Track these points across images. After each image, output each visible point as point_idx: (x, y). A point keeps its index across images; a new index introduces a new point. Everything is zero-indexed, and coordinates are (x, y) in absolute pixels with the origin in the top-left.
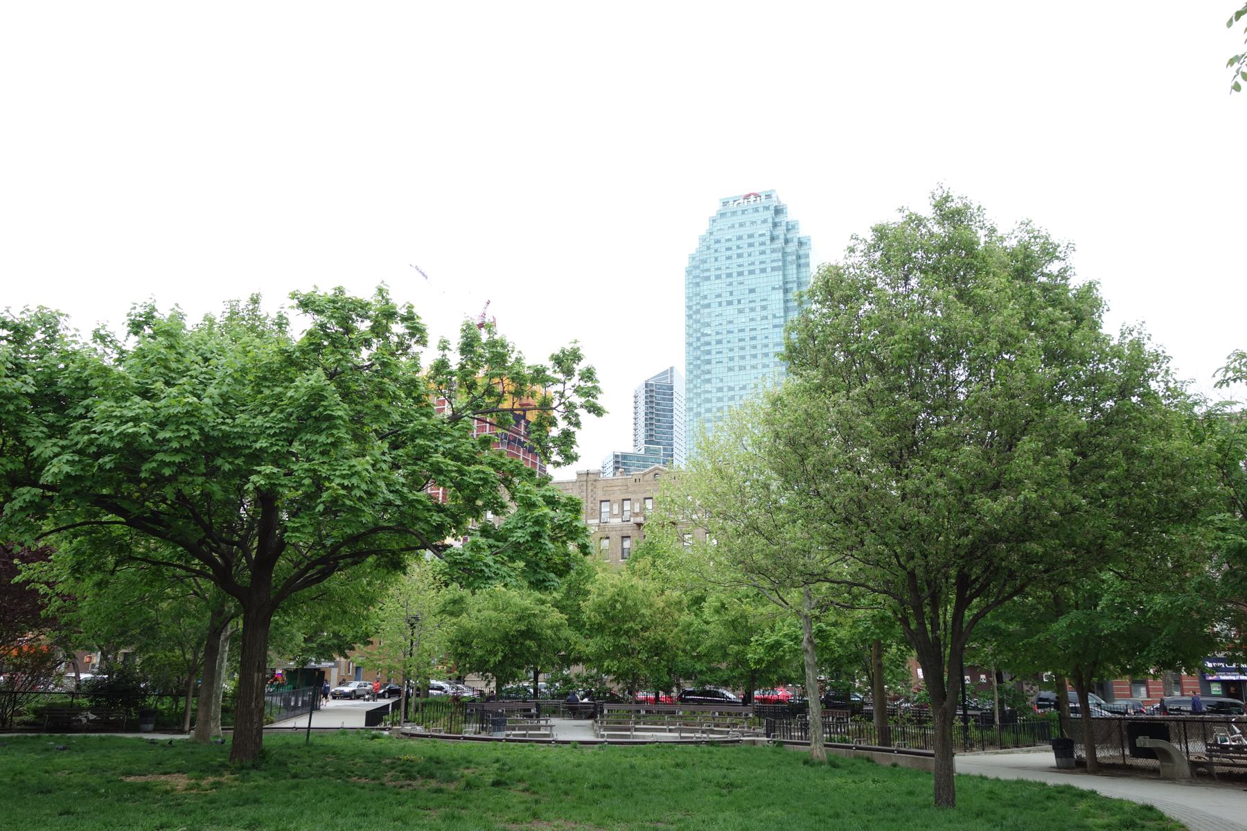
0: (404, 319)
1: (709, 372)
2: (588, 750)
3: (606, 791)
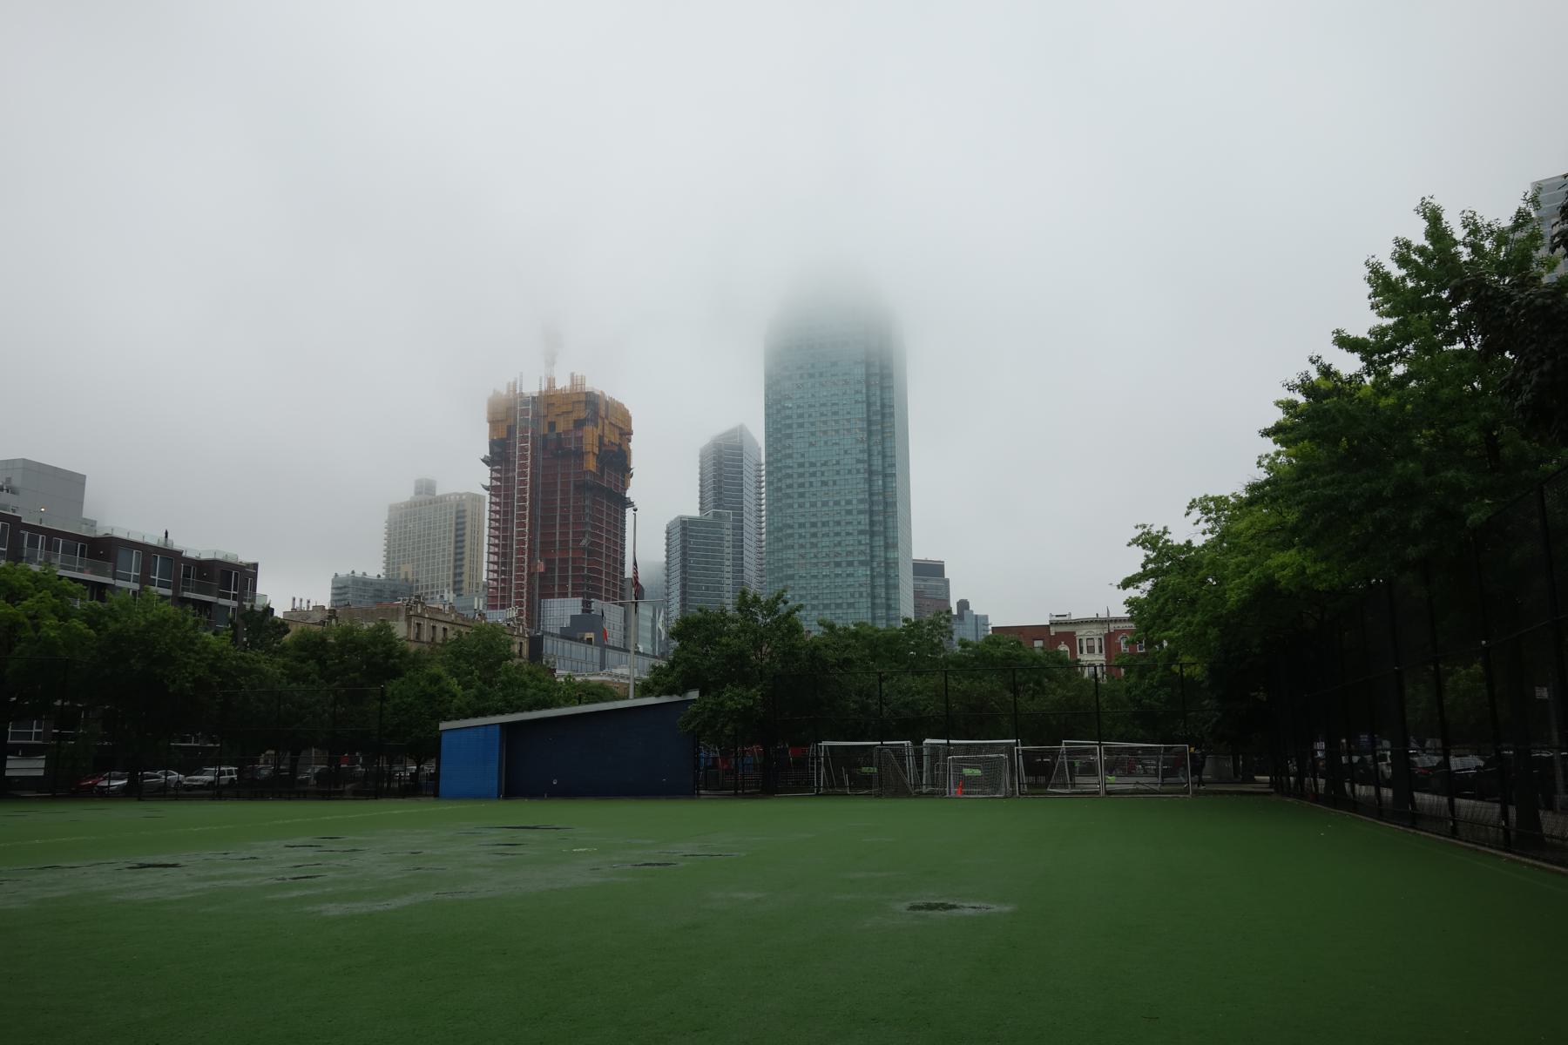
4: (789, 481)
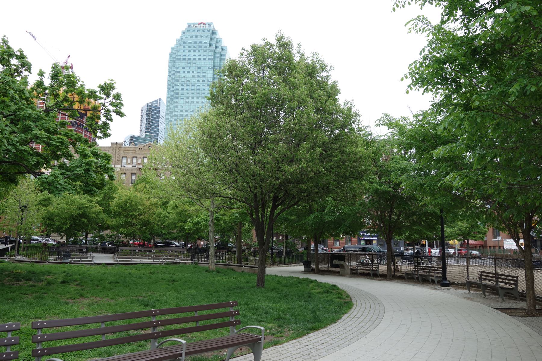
0: (17, 57)
1: (177, 103)
2: (110, 267)
3: (116, 284)
4: (176, 118)
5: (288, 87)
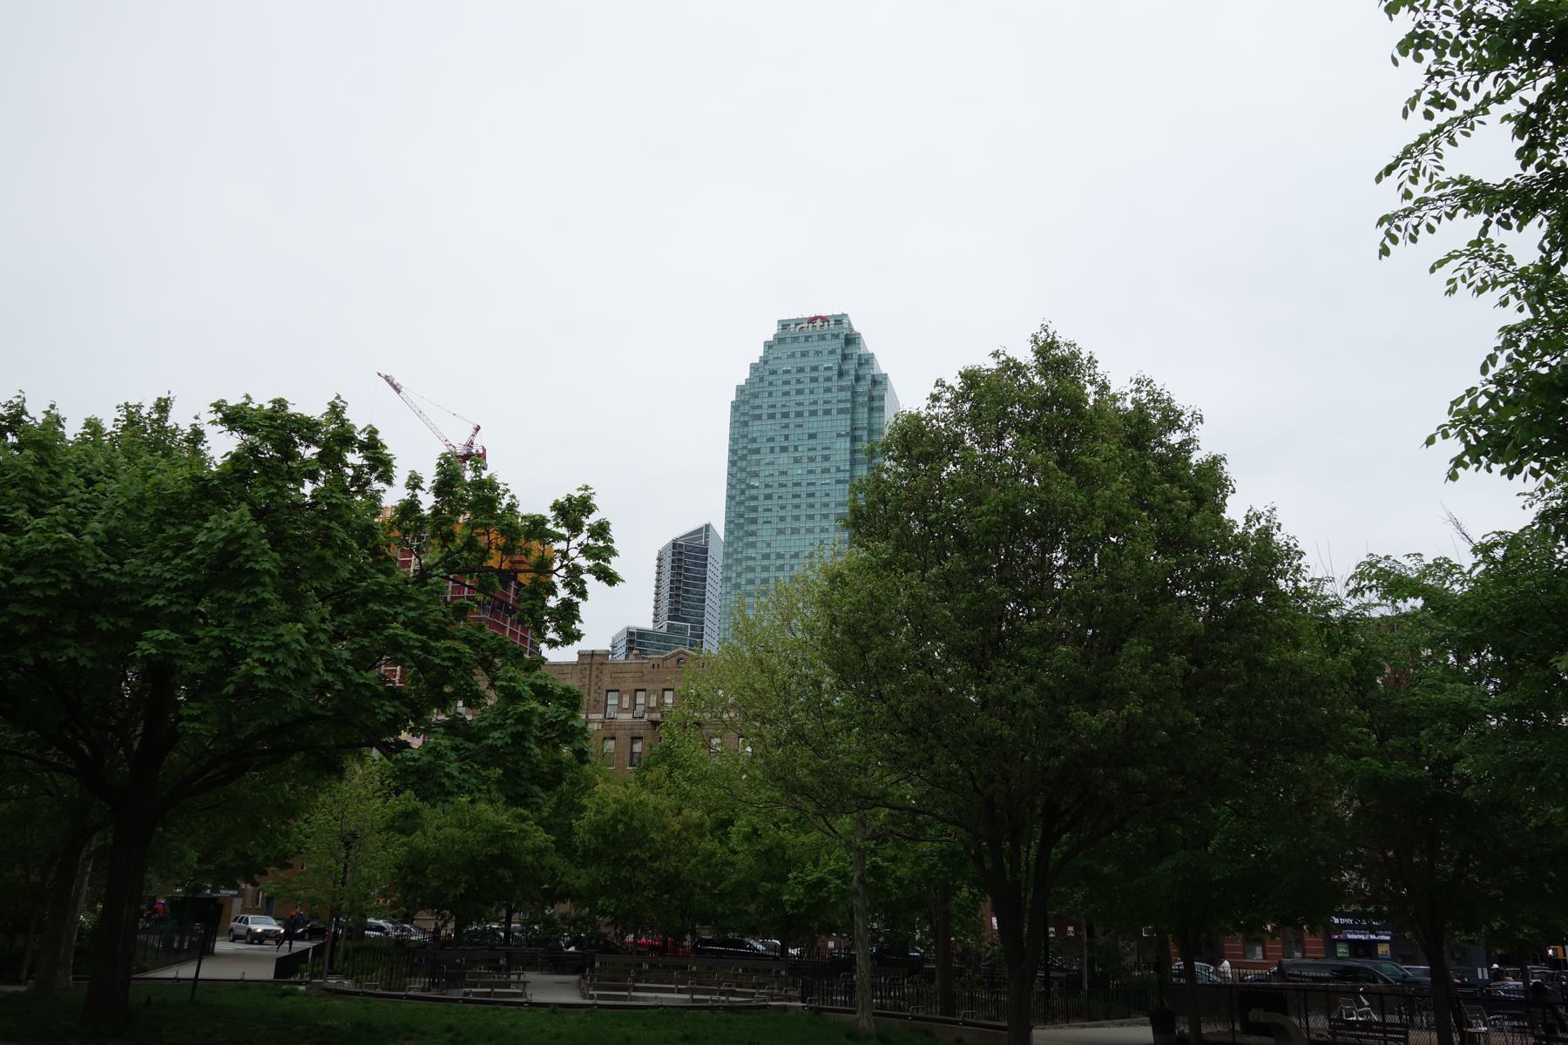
0: (363, 447)
1: (753, 534)
4: (750, 576)
5: (1073, 481)
